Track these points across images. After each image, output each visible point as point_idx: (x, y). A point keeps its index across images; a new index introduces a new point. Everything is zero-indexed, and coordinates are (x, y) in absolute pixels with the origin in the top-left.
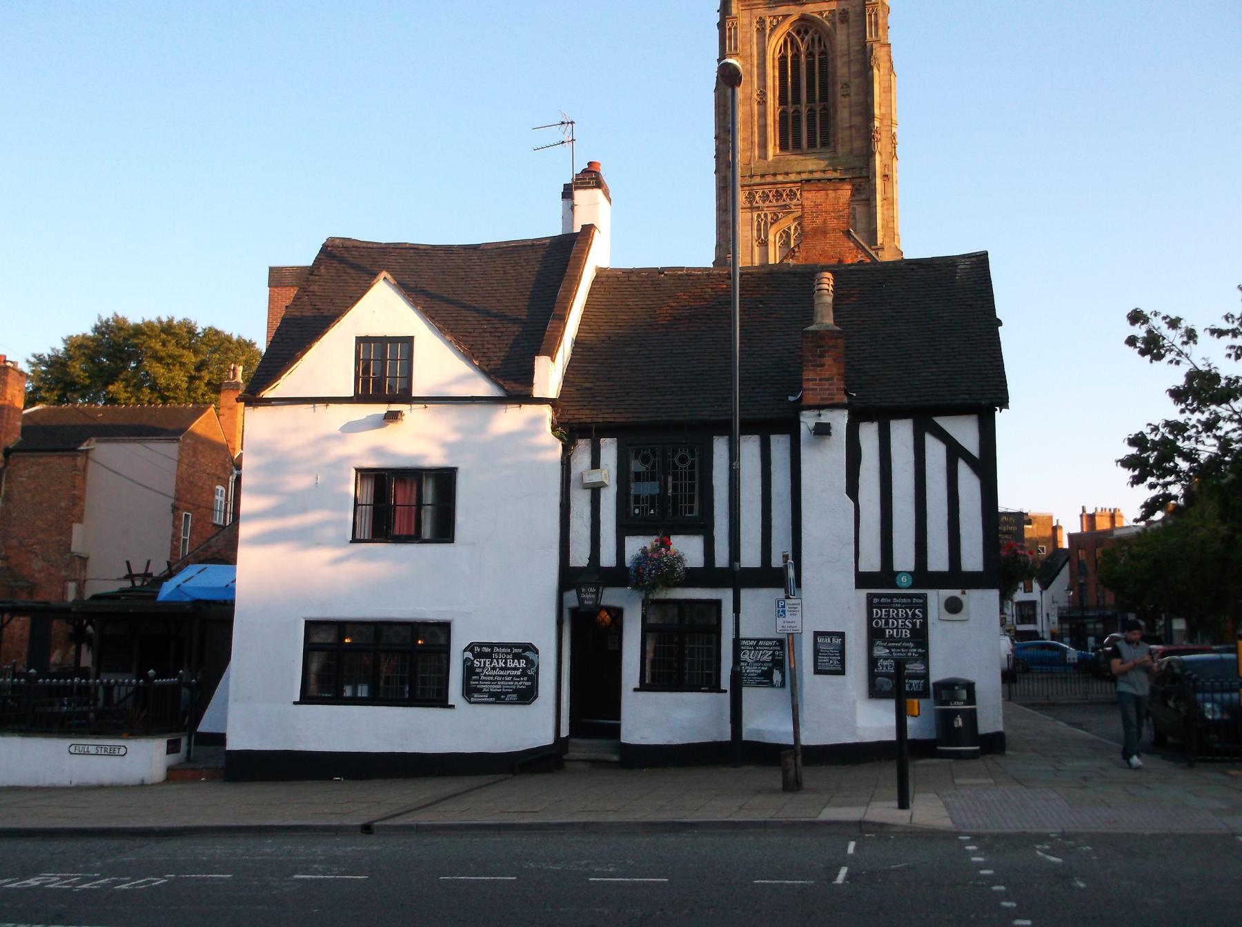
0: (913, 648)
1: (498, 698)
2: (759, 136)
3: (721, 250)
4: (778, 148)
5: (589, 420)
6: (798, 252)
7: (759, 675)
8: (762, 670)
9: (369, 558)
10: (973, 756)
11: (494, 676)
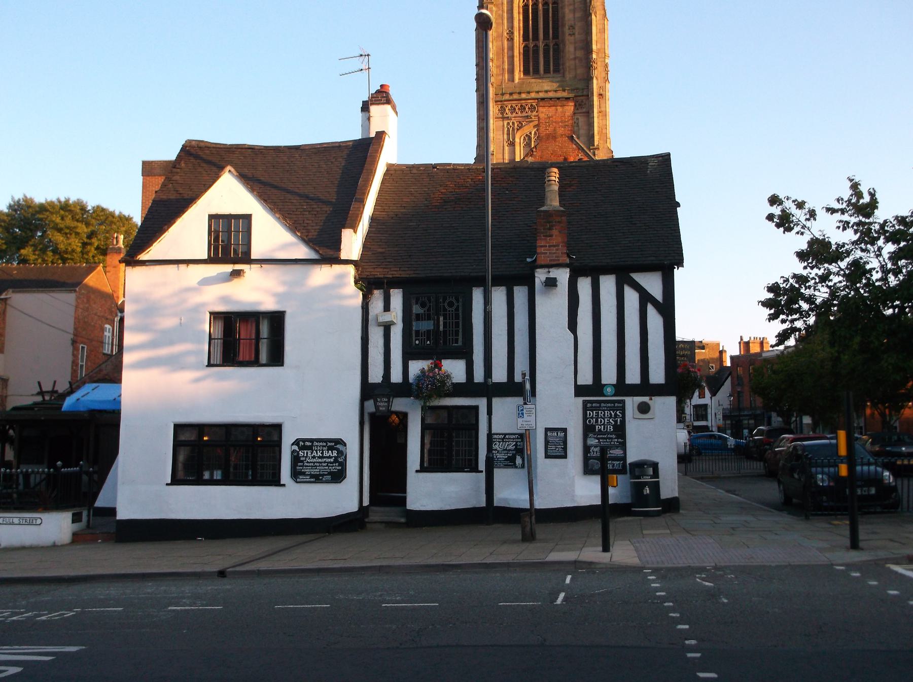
0: (615, 438)
1: (317, 479)
2: (509, 64)
6: (535, 151)
7: (506, 460)
10: (657, 514)
11: (314, 463)
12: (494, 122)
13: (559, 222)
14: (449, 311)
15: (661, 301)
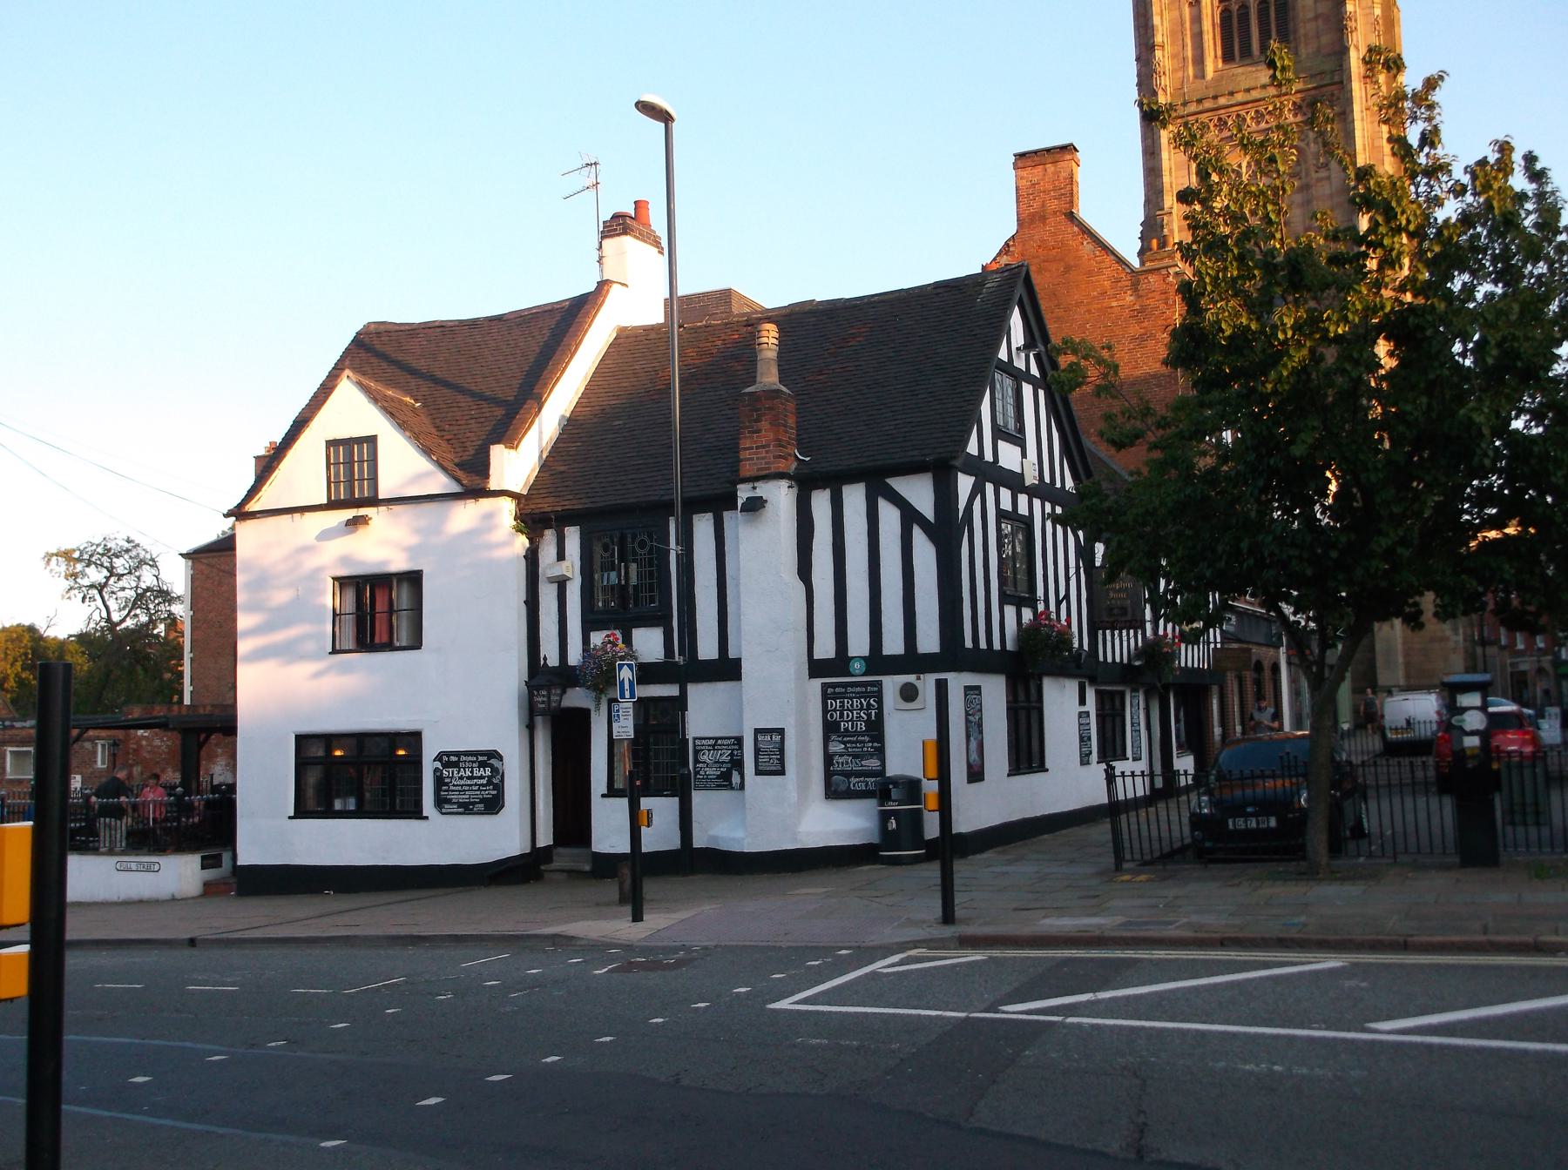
0: (869, 742)
1: (466, 809)
2: (1194, 49)
3: (1150, 206)
4: (1220, 61)
5: (549, 509)
6: (1013, 245)
7: (718, 777)
8: (722, 772)
9: (345, 670)
10: (916, 860)
11: (462, 786)
12: (1170, 155)
13: (769, 408)
14: (641, 555)
15: (932, 521)
